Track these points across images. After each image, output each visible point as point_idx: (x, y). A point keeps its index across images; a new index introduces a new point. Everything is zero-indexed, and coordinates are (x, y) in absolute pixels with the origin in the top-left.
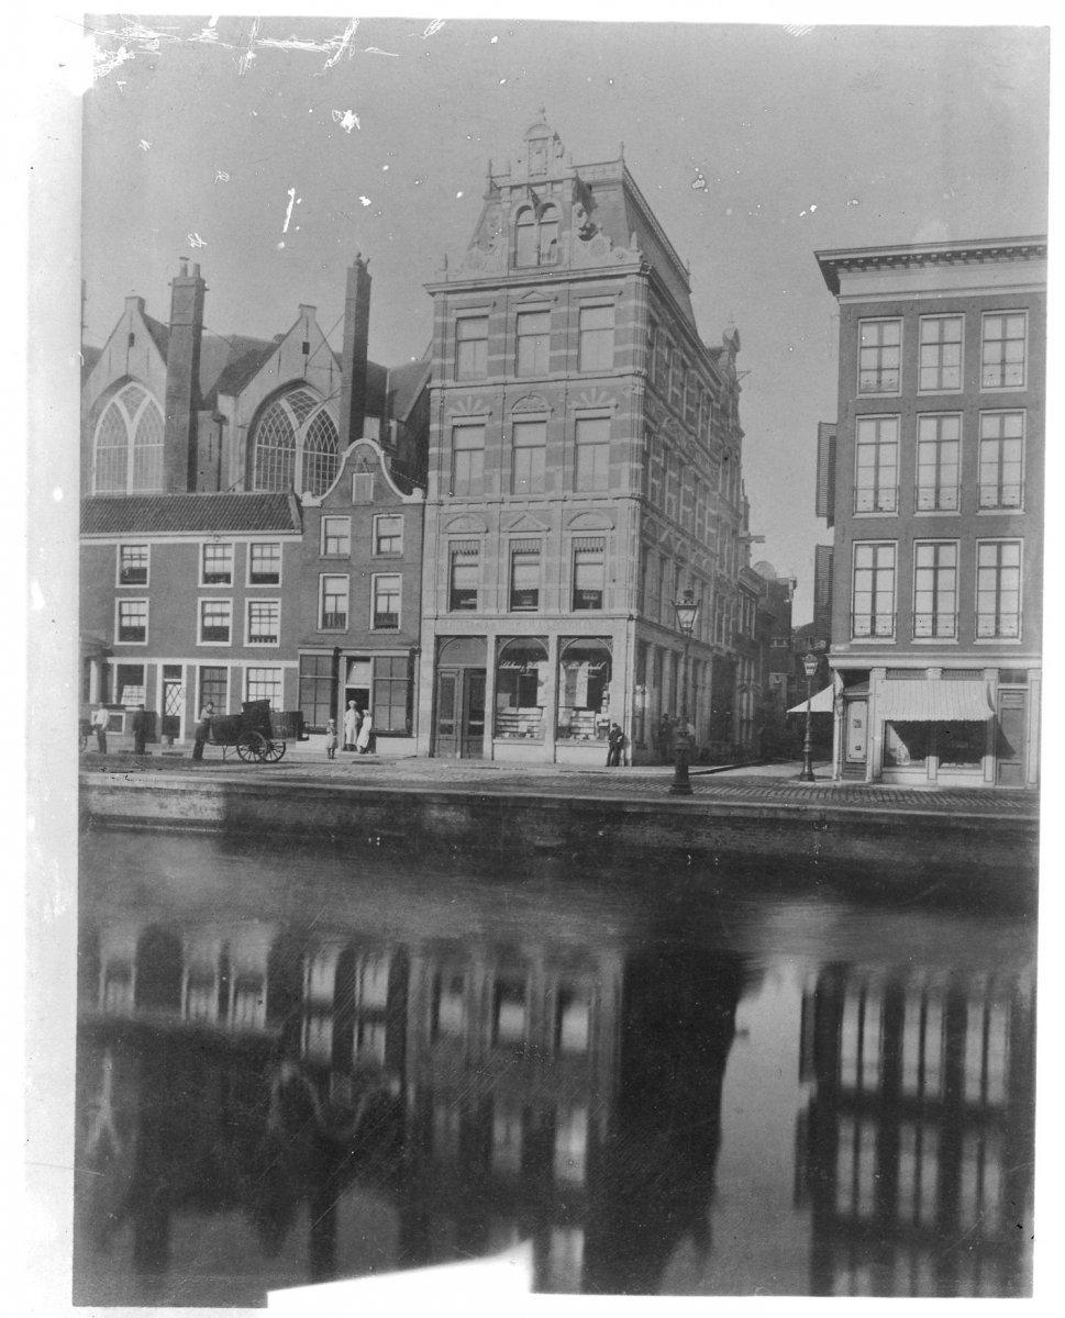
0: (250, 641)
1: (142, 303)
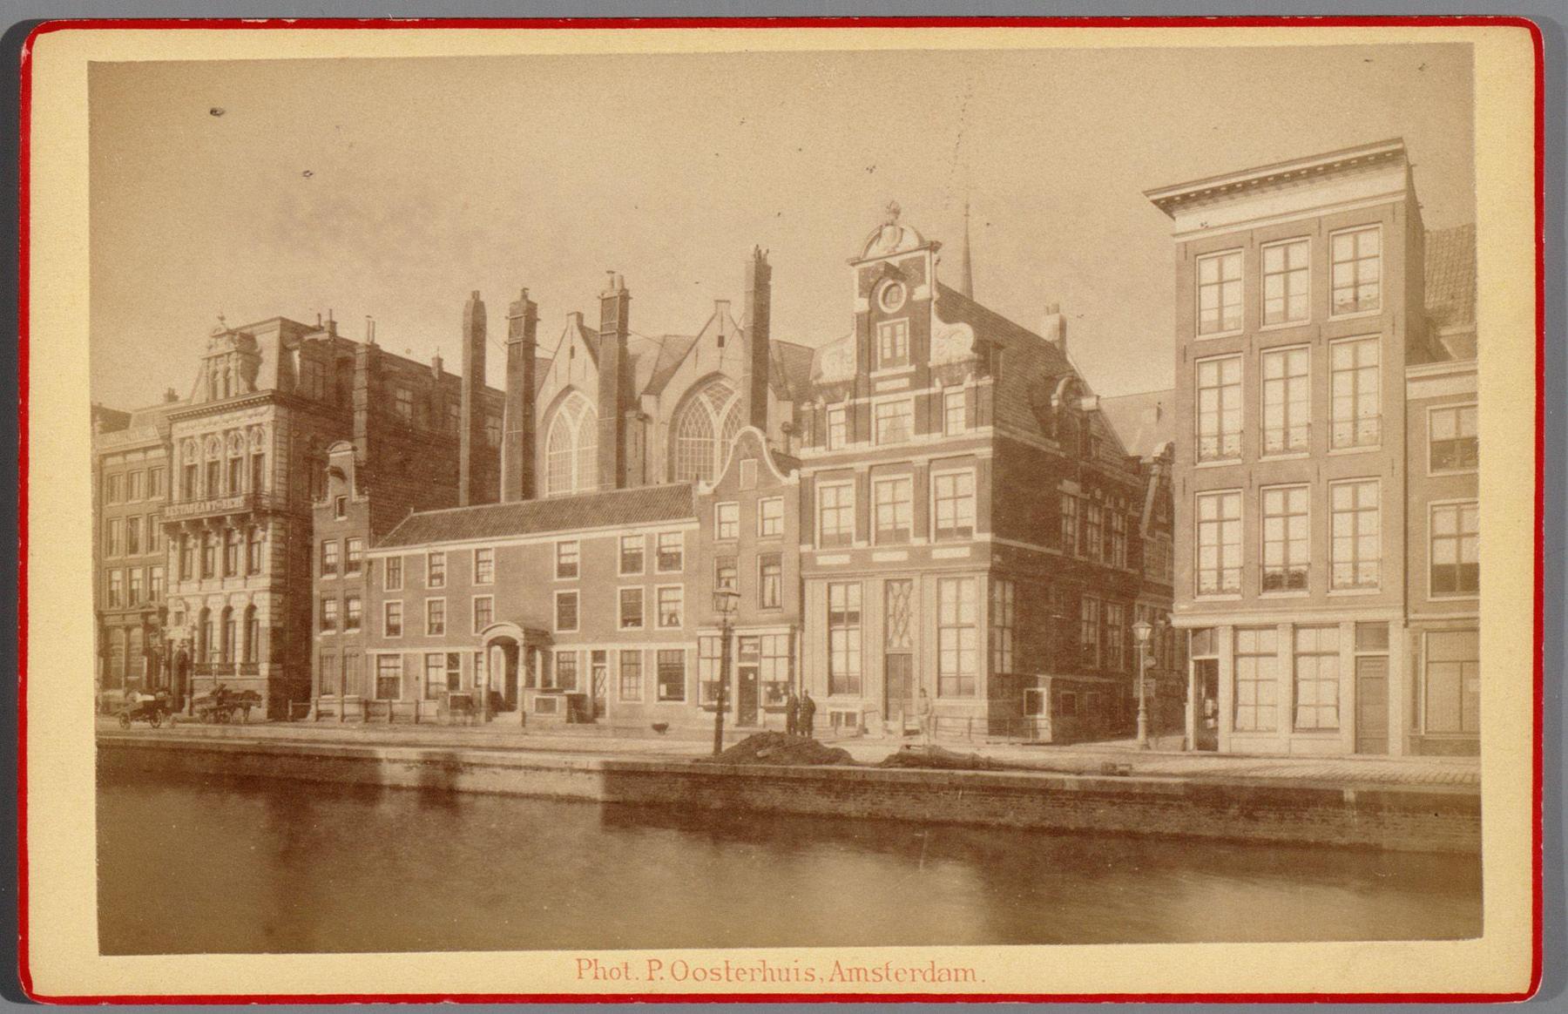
0: (677, 623)
1: (580, 317)
